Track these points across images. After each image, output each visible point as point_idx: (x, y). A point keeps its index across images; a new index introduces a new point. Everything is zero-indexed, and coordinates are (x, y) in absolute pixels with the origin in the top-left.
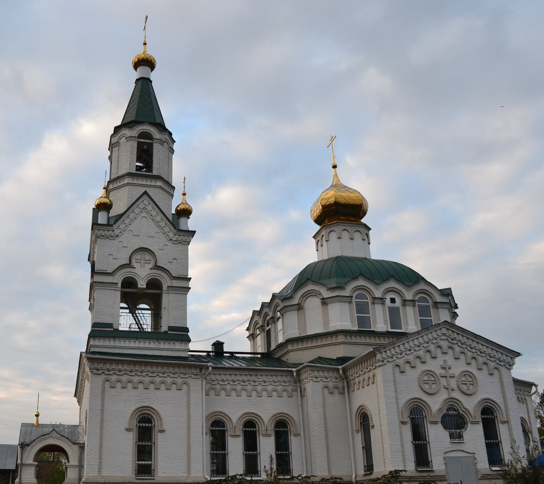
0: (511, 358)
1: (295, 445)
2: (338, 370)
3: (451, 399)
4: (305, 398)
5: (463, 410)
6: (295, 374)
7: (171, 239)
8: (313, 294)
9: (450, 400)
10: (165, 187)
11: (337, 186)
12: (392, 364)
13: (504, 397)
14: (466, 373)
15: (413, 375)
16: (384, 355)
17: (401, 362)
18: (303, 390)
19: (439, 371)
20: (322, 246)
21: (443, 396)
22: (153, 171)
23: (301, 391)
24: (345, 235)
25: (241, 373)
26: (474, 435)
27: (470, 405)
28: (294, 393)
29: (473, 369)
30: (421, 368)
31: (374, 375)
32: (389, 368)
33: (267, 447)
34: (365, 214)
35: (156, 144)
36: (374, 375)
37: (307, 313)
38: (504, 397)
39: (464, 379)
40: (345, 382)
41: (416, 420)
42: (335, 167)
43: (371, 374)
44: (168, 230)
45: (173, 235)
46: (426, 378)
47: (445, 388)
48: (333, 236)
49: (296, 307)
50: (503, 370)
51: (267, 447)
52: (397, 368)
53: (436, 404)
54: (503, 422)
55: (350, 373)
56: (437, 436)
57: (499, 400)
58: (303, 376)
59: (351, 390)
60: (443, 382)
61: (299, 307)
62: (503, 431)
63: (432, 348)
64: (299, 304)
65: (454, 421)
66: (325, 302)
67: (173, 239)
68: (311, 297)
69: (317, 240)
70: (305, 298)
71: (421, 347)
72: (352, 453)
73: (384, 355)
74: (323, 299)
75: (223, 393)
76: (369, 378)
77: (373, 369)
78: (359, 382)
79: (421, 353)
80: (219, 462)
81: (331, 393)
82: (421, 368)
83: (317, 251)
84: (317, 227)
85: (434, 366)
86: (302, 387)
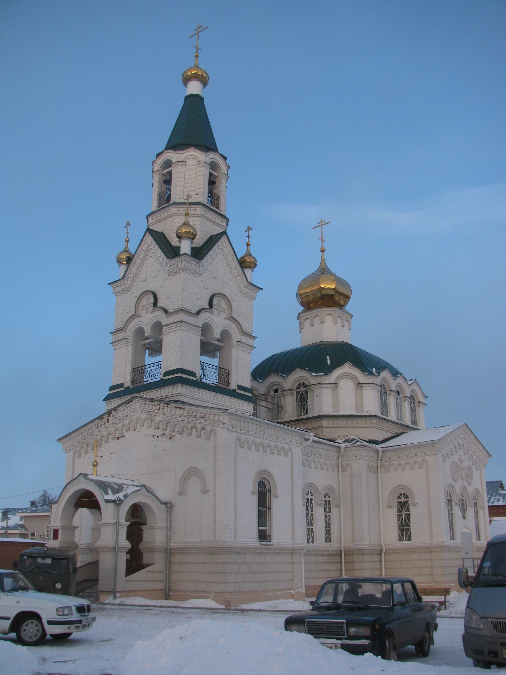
13: (482, 488)
38: (482, 488)
42: (323, 251)
49: (333, 386)
66: (359, 385)
68: (346, 379)
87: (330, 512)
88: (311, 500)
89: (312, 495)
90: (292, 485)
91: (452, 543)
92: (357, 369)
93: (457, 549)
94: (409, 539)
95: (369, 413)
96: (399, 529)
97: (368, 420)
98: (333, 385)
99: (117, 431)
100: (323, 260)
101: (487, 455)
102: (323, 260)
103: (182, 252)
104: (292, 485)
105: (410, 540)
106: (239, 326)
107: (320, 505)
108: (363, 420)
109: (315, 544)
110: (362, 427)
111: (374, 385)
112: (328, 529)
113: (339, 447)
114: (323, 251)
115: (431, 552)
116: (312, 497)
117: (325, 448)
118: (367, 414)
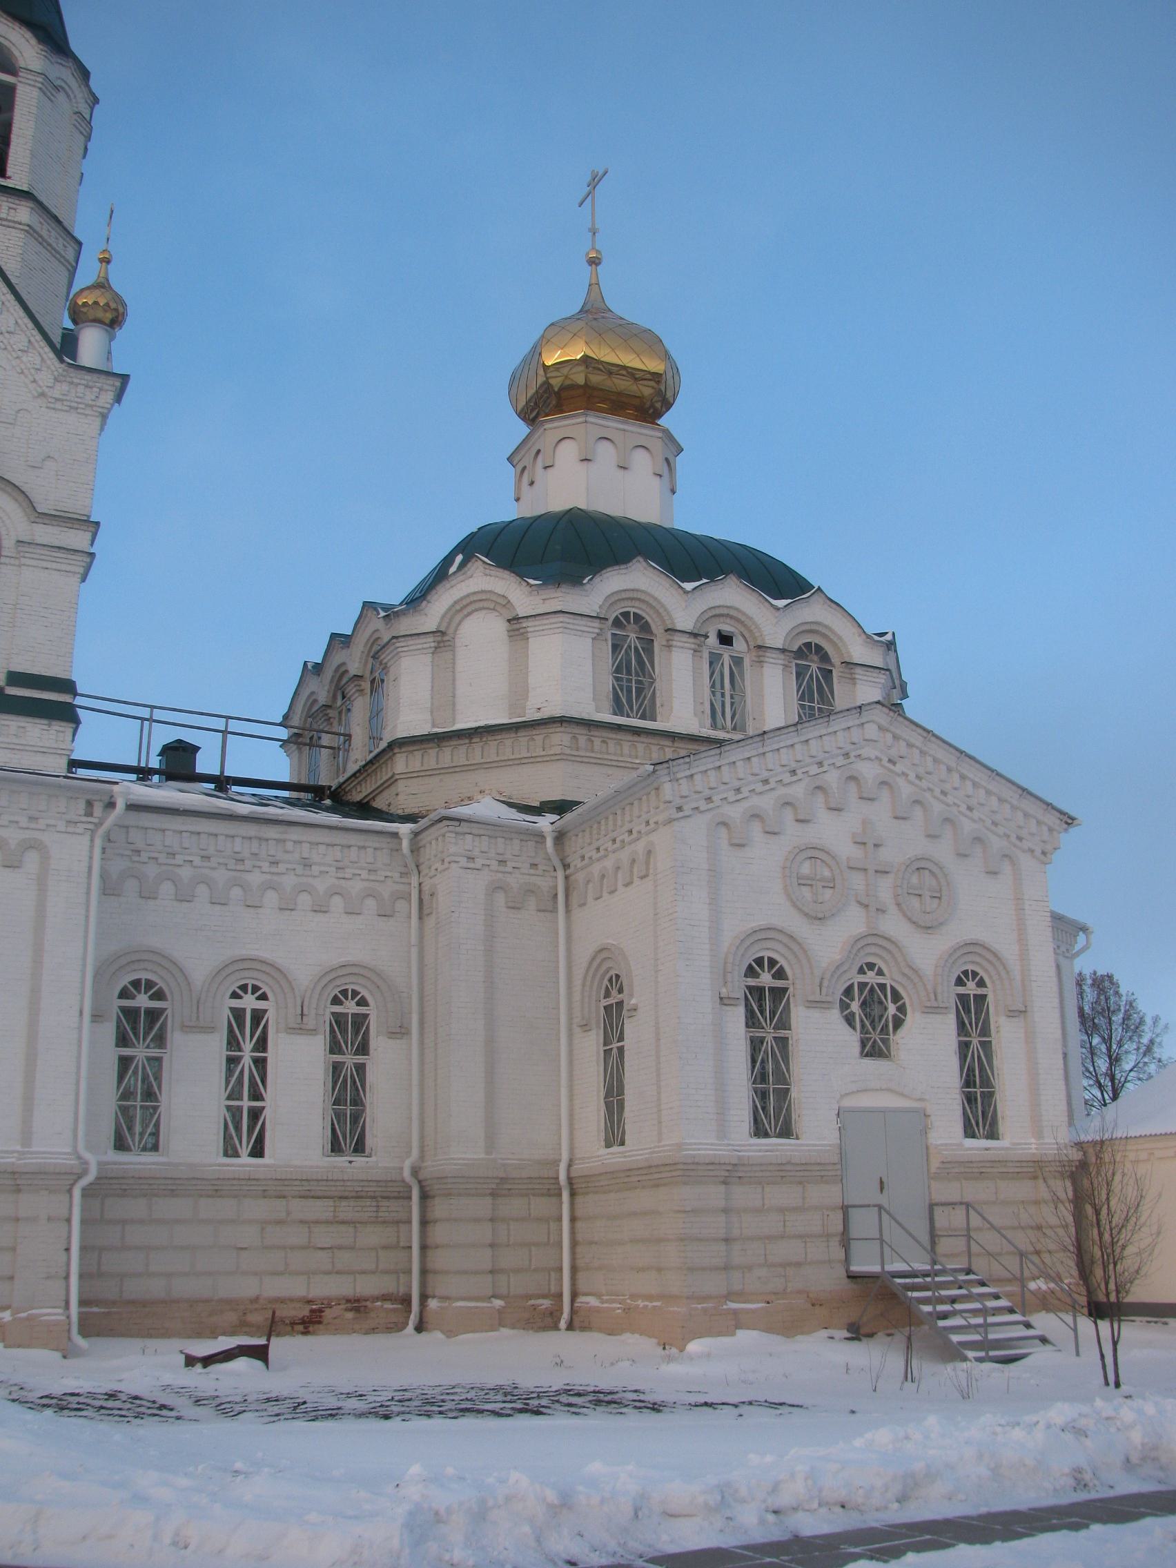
0: (1051, 830)
1: (386, 1064)
2: (540, 837)
3: (873, 938)
4: (430, 922)
5: (906, 971)
6: (405, 844)
7: (43, 395)
8: (485, 604)
9: (870, 940)
10: (44, 233)
11: (594, 316)
12: (709, 816)
13: (1022, 940)
14: (920, 866)
15: (766, 857)
16: (685, 787)
17: (734, 813)
18: (426, 897)
19: (846, 850)
20: (532, 483)
21: (853, 923)
22: (10, 171)
23: (421, 901)
24: (605, 452)
25: (232, 832)
26: (928, 1043)
27: (925, 956)
28: (401, 905)
29: (943, 851)
30: (793, 835)
31: (649, 852)
32: (695, 830)
33: (298, 1071)
34: (668, 405)
35: (28, 89)
36: (649, 852)
37: (461, 653)
38: (1022, 940)
39: (915, 880)
40: (560, 874)
41: (765, 999)
42: (594, 262)
43: (640, 847)
44: (38, 360)
45: (50, 382)
46: (806, 869)
47: (859, 902)
48: (568, 452)
49: (430, 642)
50: (1026, 861)
51: (298, 1071)
52: (723, 832)
53: (827, 947)
54: (1013, 1014)
55: (575, 846)
56: (820, 1041)
57: (1008, 949)
58: (429, 853)
59: (574, 901)
60: (857, 881)
61: (442, 639)
62: (1006, 1036)
63: (832, 778)
64: (439, 633)
65: (874, 1014)
66: (516, 625)
67: (49, 392)
68: (481, 614)
69: (520, 467)
70: (460, 616)
71: (800, 776)
72: (564, 1092)
73: (685, 787)
74: (514, 620)
75: (167, 888)
76: (634, 861)
77: (648, 833)
78: (603, 876)
79: (798, 791)
80: (137, 1110)
81: (514, 907)
82: (793, 835)
83: (517, 500)
84: (523, 429)
85: (834, 832)
86: (426, 888)
87: (363, 1049)
88: (153, 1015)
89: (263, 997)
90: (38, 962)
91: (615, 1157)
92: (506, 574)
93: (785, 1173)
94: (993, 1135)
95: (545, 713)
96: (363, 1105)
97: (539, 736)
98: (430, 639)
99: (591, 885)
100: (594, 285)
101: (1052, 819)
102: (594, 285)
103: (664, 421)
104: (38, 962)
105: (155, 1148)
106: (21, 498)
107: (300, 1028)
108: (523, 737)
109: (266, 1160)
110: (520, 762)
111: (561, 618)
112: (246, 1103)
113: (395, 835)
114: (594, 262)
115: (19, 1191)
116: (261, 1005)
117: (327, 840)
118: (537, 716)
